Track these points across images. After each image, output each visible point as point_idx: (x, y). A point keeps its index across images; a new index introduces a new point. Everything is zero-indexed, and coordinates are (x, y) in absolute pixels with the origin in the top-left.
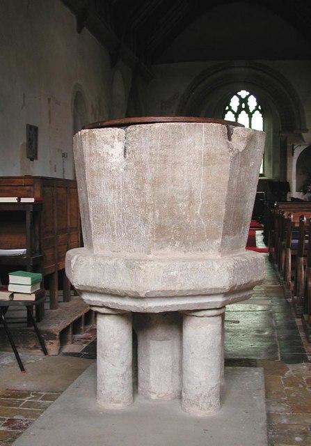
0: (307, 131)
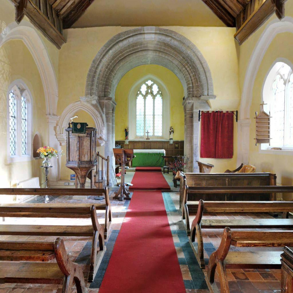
0: (215, 97)
